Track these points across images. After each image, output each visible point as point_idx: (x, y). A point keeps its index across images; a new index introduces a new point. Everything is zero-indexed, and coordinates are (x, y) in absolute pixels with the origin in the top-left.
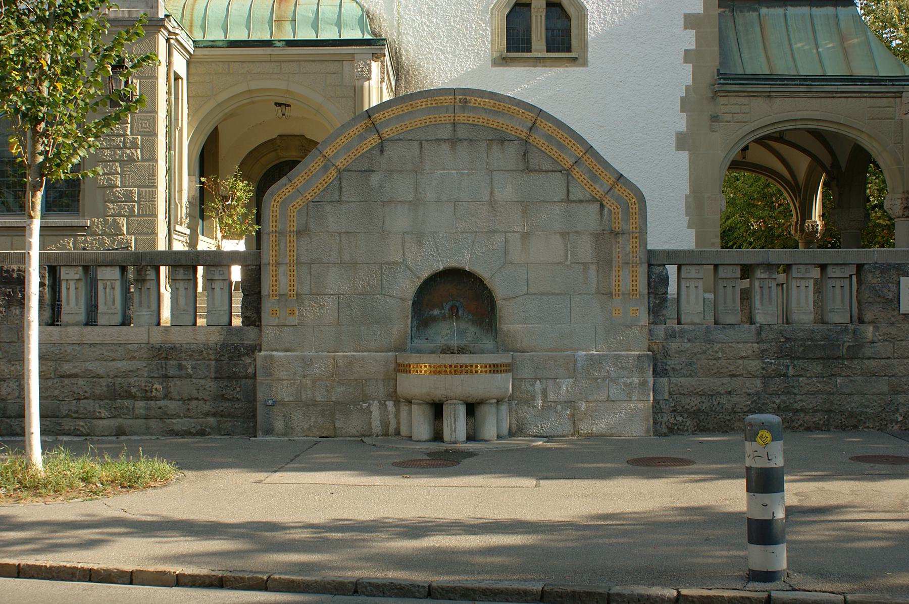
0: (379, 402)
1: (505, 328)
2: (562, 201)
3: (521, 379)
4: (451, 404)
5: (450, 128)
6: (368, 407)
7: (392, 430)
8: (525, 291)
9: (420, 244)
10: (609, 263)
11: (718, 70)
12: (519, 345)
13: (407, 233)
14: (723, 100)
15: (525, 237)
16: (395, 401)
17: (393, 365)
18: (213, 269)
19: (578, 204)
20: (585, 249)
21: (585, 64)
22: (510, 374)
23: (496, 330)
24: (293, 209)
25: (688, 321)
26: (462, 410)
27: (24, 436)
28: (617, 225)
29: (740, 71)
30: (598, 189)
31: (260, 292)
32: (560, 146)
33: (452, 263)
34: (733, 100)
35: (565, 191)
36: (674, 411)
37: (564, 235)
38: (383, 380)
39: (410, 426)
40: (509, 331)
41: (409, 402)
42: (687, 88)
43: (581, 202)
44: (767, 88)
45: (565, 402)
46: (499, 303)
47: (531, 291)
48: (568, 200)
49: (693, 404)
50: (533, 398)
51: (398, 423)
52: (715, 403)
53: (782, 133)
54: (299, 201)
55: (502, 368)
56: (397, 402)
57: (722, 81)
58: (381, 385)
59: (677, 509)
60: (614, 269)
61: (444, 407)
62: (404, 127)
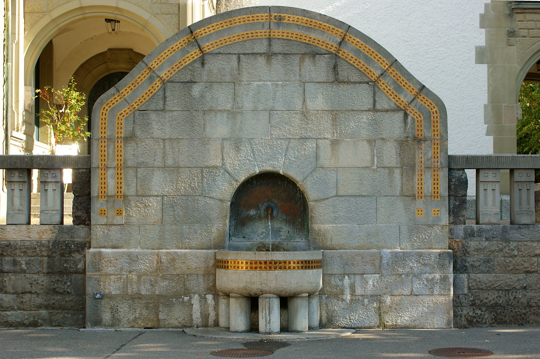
1: (316, 227)
2: (369, 110)
4: (266, 298)
7: (211, 321)
10: (413, 167)
12: (329, 243)
14: (519, 17)
15: (335, 143)
19: (384, 113)
20: (390, 154)
22: (320, 271)
25: (486, 221)
26: (276, 304)
28: (420, 133)
31: (89, 194)
32: (367, 59)
34: (529, 16)
35: (371, 101)
36: (473, 305)
38: (203, 275)
39: (228, 318)
40: (320, 230)
41: (227, 295)
43: (387, 111)
45: (372, 296)
46: (311, 204)
47: (340, 193)
48: (374, 109)
49: (491, 298)
50: (342, 293)
52: (512, 298)
55: (314, 265)
56: (216, 296)
58: (201, 280)
60: (417, 173)
61: (260, 301)
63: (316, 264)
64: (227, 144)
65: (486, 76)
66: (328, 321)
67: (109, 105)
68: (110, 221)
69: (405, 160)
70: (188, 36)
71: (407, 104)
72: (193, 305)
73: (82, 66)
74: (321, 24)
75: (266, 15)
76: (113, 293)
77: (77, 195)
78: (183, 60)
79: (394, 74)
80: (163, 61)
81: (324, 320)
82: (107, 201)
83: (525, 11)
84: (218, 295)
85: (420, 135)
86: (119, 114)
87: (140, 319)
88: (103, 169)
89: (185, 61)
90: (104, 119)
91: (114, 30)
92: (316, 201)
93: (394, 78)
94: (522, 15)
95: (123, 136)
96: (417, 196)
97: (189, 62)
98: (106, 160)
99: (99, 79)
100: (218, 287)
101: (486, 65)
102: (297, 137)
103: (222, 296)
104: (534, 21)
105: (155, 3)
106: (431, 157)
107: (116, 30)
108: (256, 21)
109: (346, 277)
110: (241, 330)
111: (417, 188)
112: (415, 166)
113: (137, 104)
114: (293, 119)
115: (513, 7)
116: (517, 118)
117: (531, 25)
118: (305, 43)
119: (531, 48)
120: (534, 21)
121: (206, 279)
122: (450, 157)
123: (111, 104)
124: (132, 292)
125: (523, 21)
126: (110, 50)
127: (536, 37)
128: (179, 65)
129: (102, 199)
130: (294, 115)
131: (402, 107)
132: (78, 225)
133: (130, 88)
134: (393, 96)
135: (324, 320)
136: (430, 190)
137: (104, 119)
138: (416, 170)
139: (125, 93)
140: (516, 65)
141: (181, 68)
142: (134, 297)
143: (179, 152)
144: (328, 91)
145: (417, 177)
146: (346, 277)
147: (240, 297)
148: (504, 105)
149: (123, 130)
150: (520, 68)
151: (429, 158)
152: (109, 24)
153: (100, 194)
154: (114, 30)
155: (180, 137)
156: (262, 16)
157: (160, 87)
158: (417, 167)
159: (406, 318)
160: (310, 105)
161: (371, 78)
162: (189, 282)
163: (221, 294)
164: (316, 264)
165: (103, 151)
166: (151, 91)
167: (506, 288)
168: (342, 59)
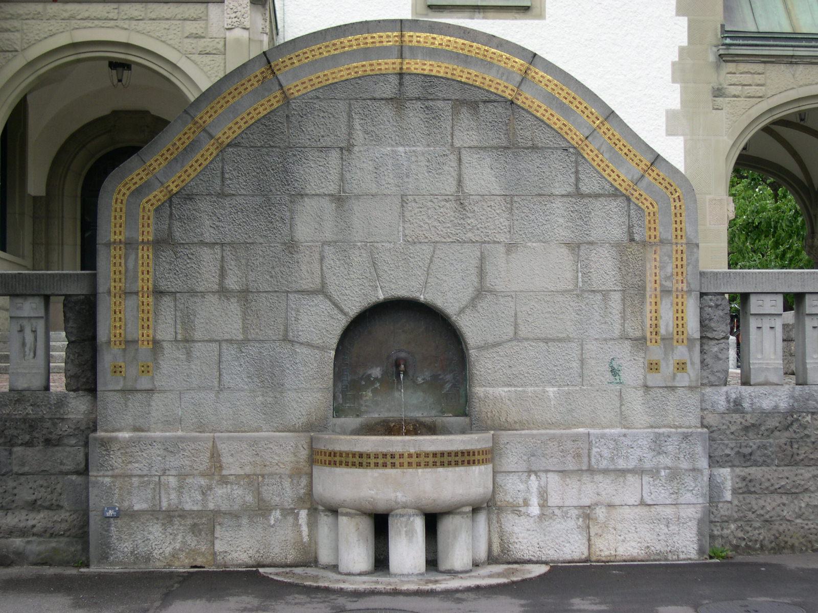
1: (479, 391)
4: (402, 516)
5: (394, 80)
8: (511, 334)
11: (723, 26)
13: (329, 243)
14: (731, 67)
16: (309, 509)
18: (19, 301)
20: (604, 267)
21: (541, 16)
22: (490, 466)
24: (148, 206)
25: (761, 379)
26: (419, 525)
27: (95, 269)
28: (652, 233)
29: (751, 28)
30: (622, 177)
31: (94, 338)
32: (564, 109)
34: (743, 67)
37: (574, 247)
38: (290, 476)
39: (336, 550)
41: (334, 511)
42: (682, 50)
43: (597, 196)
44: (790, 53)
46: (473, 353)
48: (578, 194)
49: (769, 508)
50: (526, 503)
53: (802, 115)
54: (157, 195)
55: (481, 457)
56: (313, 511)
57: (728, 41)
58: (287, 484)
59: (335, 385)
60: (648, 300)
61: (391, 521)
62: (322, 79)
63: (481, 457)
64: (329, 251)
65: (683, 155)
66: (502, 551)
67: (128, 186)
68: (129, 385)
69: (629, 278)
70: (263, 69)
71: (631, 184)
73: (73, 137)
74: (487, 51)
75: (395, 34)
76: (136, 508)
77: (73, 339)
78: (255, 110)
79: (609, 134)
80: (220, 111)
81: (496, 549)
82: (124, 350)
83: (737, 59)
84: (316, 509)
85: (653, 237)
86: (145, 200)
87: (183, 551)
88: (118, 295)
89: (257, 111)
90: (118, 210)
91: (120, 81)
92: (480, 348)
93: (609, 141)
94: (734, 65)
95: (151, 238)
96: (648, 339)
97: (265, 112)
98: (123, 280)
99: (98, 156)
100: (315, 496)
101: (682, 138)
103: (323, 511)
104: (751, 73)
105: (187, 37)
106: (672, 275)
107: (124, 81)
108: (378, 45)
109: (533, 477)
110: (358, 571)
111: (648, 326)
112: (644, 289)
113: (175, 184)
114: (442, 210)
115: (721, 52)
116: (728, 217)
117: (747, 78)
118: (461, 82)
119: (747, 113)
120: (751, 73)
121: (295, 481)
122: (702, 274)
123: (131, 185)
124: (169, 505)
125: (735, 73)
126: (115, 113)
127: (753, 97)
128: (247, 118)
129: (116, 347)
130: (443, 203)
131: (622, 189)
132: (74, 391)
133: (164, 157)
134: (608, 171)
135: (496, 549)
136: (671, 329)
137: (118, 210)
138: (648, 296)
139: (155, 165)
140: (726, 138)
141: (251, 122)
142: (172, 514)
143: (247, 265)
144: (500, 163)
145: (648, 308)
146: (533, 477)
147: (358, 515)
148: (708, 197)
149: (151, 229)
150: (731, 143)
151: (669, 274)
152: (114, 72)
153: (113, 339)
154: (120, 81)
155: (249, 241)
156: (388, 36)
157: (214, 154)
158: (648, 289)
159: (634, 544)
160: (470, 186)
161: (571, 141)
162: (265, 488)
163: (320, 508)
164: (484, 457)
165: (118, 264)
166: (199, 162)
167: (793, 490)
168: (523, 109)
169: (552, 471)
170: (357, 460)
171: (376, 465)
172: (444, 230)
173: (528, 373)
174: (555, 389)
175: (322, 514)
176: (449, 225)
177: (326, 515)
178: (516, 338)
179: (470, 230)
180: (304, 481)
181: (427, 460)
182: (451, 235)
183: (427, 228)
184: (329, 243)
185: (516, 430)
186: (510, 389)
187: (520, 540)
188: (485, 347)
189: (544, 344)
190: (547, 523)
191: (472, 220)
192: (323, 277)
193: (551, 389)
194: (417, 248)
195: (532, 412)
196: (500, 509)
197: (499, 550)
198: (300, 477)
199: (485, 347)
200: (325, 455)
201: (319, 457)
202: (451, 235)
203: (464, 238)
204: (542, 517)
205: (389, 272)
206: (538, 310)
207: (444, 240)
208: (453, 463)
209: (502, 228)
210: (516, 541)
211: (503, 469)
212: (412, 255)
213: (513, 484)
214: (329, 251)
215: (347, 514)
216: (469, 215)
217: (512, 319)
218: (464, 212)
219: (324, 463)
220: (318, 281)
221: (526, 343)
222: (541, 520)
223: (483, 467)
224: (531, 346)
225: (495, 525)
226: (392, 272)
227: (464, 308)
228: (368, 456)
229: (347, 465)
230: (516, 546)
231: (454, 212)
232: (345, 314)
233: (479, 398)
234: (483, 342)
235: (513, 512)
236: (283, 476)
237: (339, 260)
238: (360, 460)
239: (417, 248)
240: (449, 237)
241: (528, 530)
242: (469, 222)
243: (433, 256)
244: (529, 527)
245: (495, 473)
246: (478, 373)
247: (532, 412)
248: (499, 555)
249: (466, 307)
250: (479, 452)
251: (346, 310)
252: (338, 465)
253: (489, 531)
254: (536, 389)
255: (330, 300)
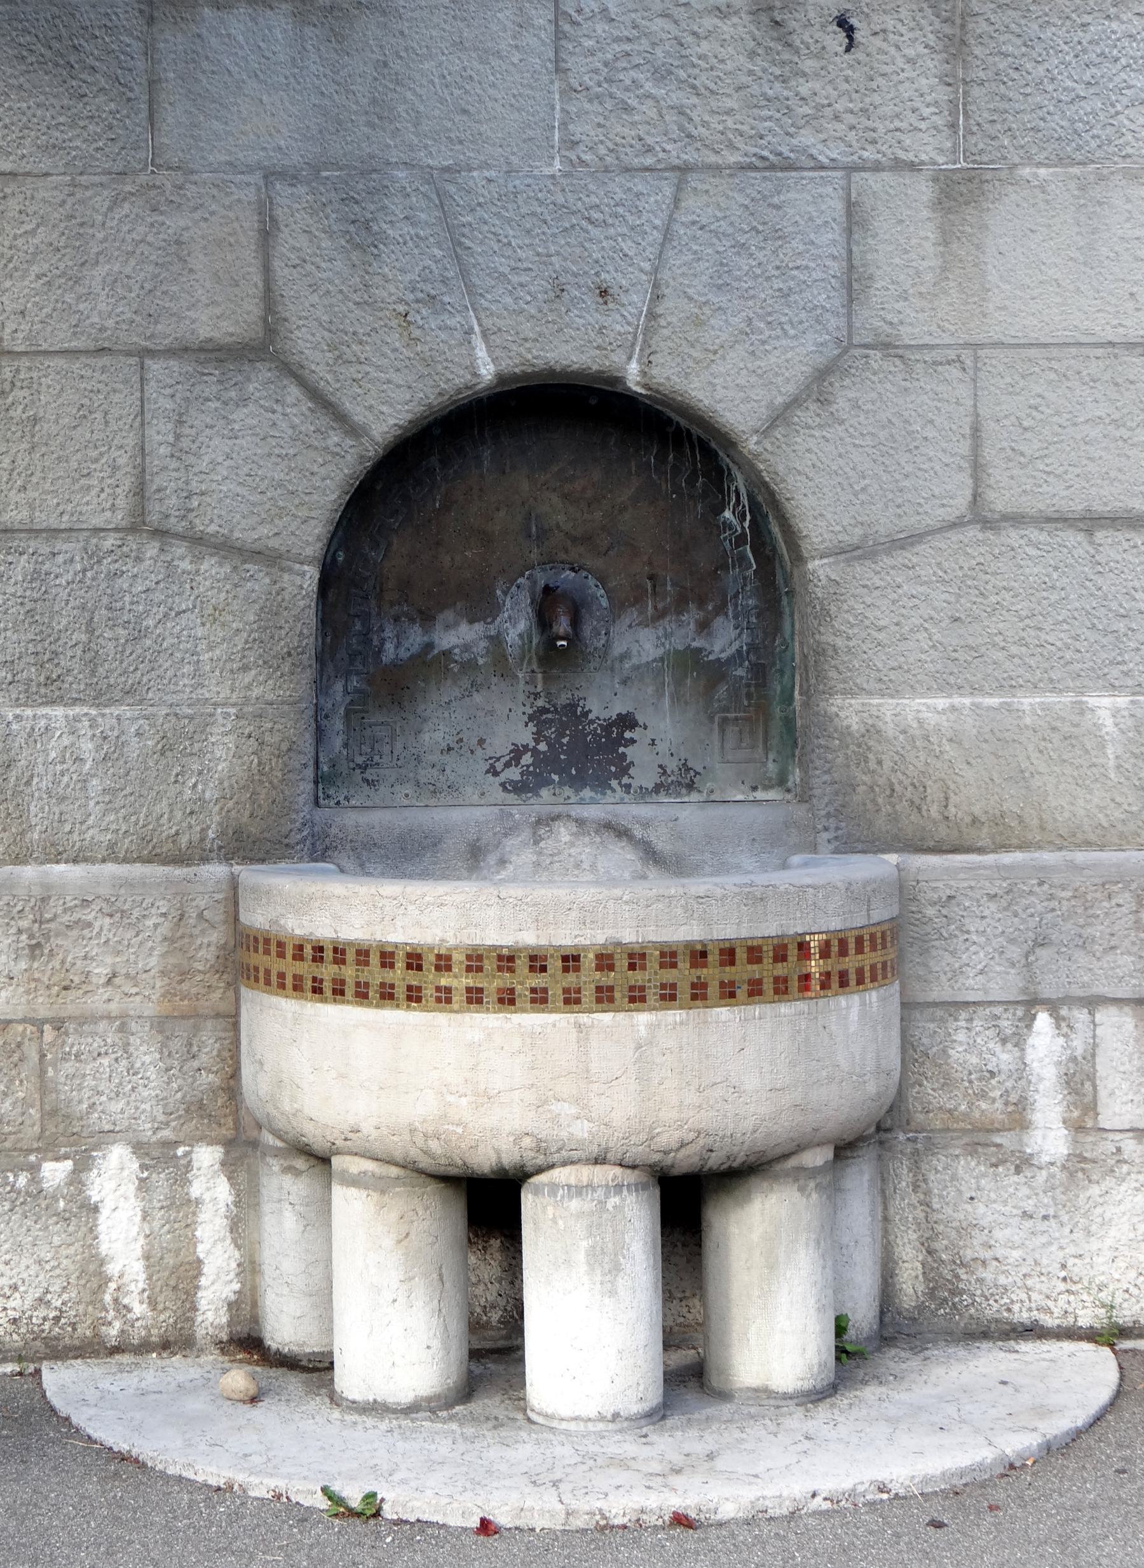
0: (139, 1148)
1: (848, 711)
3: (956, 1006)
6: (77, 1179)
8: (961, 502)
9: (363, 238)
15: (960, 193)
16: (229, 1144)
17: (216, 937)
23: (789, 723)
33: (570, 346)
38: (162, 1024)
39: (323, 1298)
40: (872, 731)
50: (1019, 1117)
51: (250, 1268)
58: (146, 1055)
61: (529, 1202)
64: (291, 202)
66: (932, 1293)
72: (95, 1209)
84: (254, 1144)
102: (733, 158)
103: (277, 1153)
109: (1043, 1020)
110: (406, 1397)
121: (176, 1045)
130: (709, 22)
146: (1043, 1020)
162: (69, 1067)
163: (269, 1139)
169: (1116, 1001)
170: (399, 975)
171: (475, 997)
172: (713, 120)
173: (1022, 642)
174: (1123, 701)
175: (275, 1165)
176: (729, 103)
177: (287, 1170)
178: (981, 516)
179: (808, 119)
180: (209, 1043)
181: (669, 976)
182: (739, 142)
183: (653, 113)
184: (291, 177)
185: (980, 851)
186: (957, 700)
187: (1000, 1252)
188: (856, 552)
189: (1081, 537)
190: (1095, 1190)
191: (817, 85)
192: (269, 299)
193: (1106, 702)
194: (612, 186)
195: (1037, 782)
196: (927, 1145)
197: (921, 1288)
198: (197, 1029)
199: (856, 552)
200: (281, 955)
201: (258, 959)
202: (739, 142)
203: (785, 150)
204: (1078, 1166)
205: (515, 279)
206: (1057, 413)
207: (713, 159)
208: (768, 986)
209: (926, 111)
210: (988, 1254)
211: (934, 995)
212: (596, 215)
213: (971, 1047)
214: (291, 202)
215: (354, 1182)
216: (809, 65)
217: (965, 447)
218: (786, 56)
219: (281, 985)
220: (252, 308)
221: (1014, 534)
222: (1072, 1175)
223: (873, 996)
224: (1030, 543)
225: (905, 1205)
226: (524, 278)
227: (787, 406)
228: (444, 963)
229: (362, 996)
230: (981, 1273)
231: (752, 55)
232: (354, 430)
233: (846, 732)
234: (859, 531)
235: (972, 1149)
236: (133, 1026)
237: (331, 234)
238: (413, 978)
239: (612, 186)
240: (731, 146)
241: (1027, 1215)
242: (804, 90)
243: (671, 219)
244: (1029, 1205)
245: (908, 1006)
246: (840, 642)
247: (1037, 782)
248: (921, 1308)
249: (795, 402)
250: (859, 940)
251: (359, 414)
252: (328, 992)
253: (886, 1219)
254: (1051, 698)
255: (302, 383)
